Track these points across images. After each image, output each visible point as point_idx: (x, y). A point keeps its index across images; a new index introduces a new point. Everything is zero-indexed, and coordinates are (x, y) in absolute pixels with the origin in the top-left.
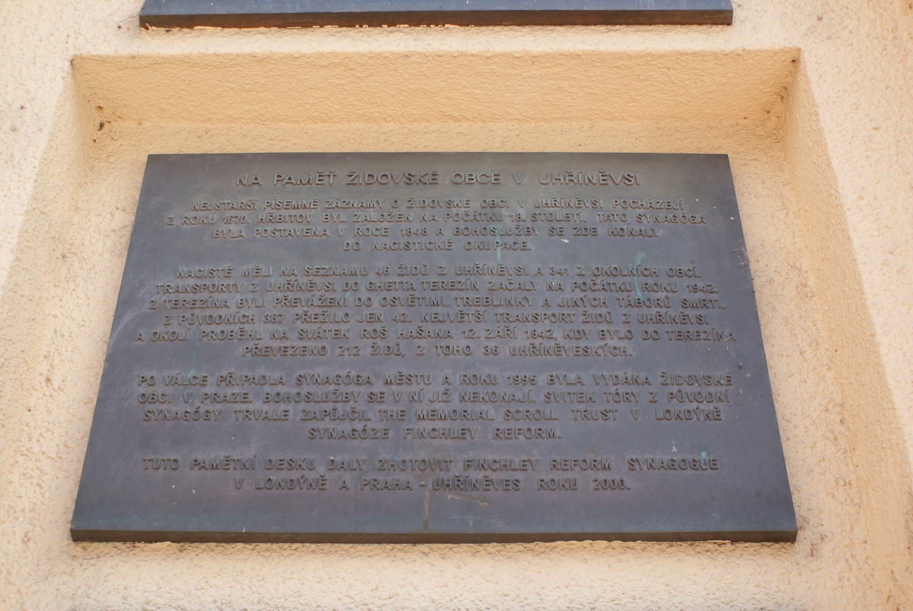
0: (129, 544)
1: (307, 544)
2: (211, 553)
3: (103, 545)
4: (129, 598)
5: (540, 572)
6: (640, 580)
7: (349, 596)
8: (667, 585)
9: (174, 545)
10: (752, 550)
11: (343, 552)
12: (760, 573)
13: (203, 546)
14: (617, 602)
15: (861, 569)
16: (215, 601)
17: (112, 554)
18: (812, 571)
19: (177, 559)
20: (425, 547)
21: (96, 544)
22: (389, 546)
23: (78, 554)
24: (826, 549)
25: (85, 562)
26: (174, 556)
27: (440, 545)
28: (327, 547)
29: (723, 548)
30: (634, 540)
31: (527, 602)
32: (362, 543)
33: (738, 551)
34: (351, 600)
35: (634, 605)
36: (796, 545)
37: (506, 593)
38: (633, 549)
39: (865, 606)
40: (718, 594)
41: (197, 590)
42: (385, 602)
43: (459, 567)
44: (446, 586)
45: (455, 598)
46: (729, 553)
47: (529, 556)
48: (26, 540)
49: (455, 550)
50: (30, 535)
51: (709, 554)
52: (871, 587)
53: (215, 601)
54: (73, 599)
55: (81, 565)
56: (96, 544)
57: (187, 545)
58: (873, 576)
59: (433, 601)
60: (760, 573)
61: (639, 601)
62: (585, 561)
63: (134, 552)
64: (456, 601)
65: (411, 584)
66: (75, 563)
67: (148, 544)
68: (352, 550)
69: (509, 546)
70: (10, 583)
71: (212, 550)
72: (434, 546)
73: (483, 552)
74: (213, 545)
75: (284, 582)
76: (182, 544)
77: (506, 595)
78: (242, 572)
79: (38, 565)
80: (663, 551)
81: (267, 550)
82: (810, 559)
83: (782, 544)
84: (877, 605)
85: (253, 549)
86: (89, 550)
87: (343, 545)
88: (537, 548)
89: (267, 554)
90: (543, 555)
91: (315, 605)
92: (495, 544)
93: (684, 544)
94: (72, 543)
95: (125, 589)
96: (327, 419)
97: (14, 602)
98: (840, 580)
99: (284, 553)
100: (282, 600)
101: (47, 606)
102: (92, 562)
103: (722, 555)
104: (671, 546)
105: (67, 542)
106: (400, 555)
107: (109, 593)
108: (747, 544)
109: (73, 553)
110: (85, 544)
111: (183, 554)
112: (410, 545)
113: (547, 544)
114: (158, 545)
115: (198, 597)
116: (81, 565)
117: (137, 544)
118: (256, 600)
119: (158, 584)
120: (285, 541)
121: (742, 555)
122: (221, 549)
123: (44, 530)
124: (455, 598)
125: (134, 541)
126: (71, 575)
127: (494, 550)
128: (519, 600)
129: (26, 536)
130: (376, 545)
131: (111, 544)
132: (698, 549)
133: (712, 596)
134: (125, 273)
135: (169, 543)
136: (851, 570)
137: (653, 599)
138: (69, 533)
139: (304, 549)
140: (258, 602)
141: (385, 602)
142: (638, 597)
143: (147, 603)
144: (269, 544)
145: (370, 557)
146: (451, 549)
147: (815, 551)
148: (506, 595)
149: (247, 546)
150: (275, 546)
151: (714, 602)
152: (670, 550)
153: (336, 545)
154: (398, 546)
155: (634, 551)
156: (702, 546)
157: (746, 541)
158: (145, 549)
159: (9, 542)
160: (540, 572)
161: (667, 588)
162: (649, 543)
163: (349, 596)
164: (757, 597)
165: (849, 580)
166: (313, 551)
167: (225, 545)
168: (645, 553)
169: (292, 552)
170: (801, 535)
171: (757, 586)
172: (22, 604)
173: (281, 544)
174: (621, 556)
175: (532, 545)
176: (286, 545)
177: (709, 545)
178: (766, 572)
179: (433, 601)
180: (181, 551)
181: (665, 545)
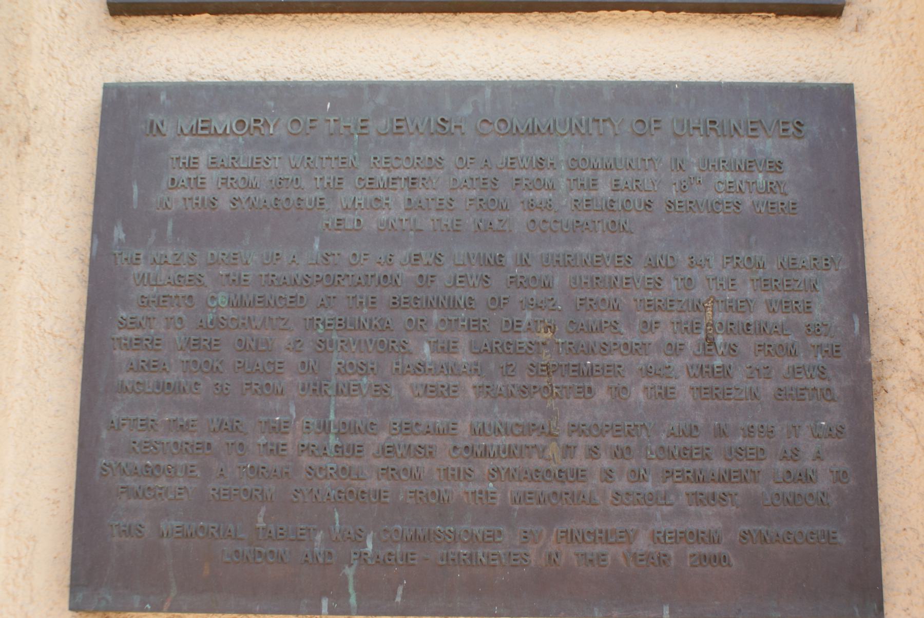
0: (167, 18)
1: (347, 14)
2: (251, 25)
3: (141, 19)
4: (173, 70)
5: (581, 42)
6: (682, 51)
7: (391, 64)
8: (708, 57)
9: (213, 17)
10: (796, 24)
11: (383, 22)
12: (802, 47)
13: (242, 18)
14: (657, 71)
15: (903, 45)
16: (258, 71)
17: (151, 27)
18: (855, 46)
19: (217, 31)
20: (466, 17)
21: (134, 19)
22: (430, 16)
23: (118, 28)
24: (871, 25)
25: (125, 36)
26: (214, 28)
27: (481, 15)
28: (367, 16)
29: (767, 22)
30: (678, 11)
31: (567, 70)
32: (403, 12)
33: (782, 25)
34: (393, 69)
35: (674, 74)
36: (842, 20)
37: (547, 61)
38: (676, 20)
39: (904, 81)
40: (758, 66)
41: (239, 60)
42: (427, 70)
43: (500, 36)
44: (487, 54)
45: (497, 65)
46: (772, 27)
47: (571, 25)
48: (63, 16)
49: (497, 19)
50: (66, 10)
51: (752, 27)
52: (912, 63)
53: (258, 71)
54: (117, 71)
55: (122, 38)
56: (134, 18)
57: (226, 17)
58: (915, 52)
59: (474, 69)
60: (802, 47)
61: (679, 71)
62: (627, 31)
63: (173, 25)
64: (496, 69)
65: (452, 52)
66: (116, 38)
67: (186, 17)
68: (393, 20)
69: (551, 16)
70: (53, 58)
71: (252, 22)
72: (475, 15)
73: (524, 22)
74: (251, 16)
75: (325, 51)
76: (221, 16)
77: (547, 64)
78: (283, 43)
79: (78, 40)
80: (706, 23)
81: (307, 21)
82: (854, 34)
83: (827, 18)
84: (915, 80)
85: (292, 20)
86: (127, 24)
87: (383, 15)
88: (579, 18)
89: (307, 24)
90: (585, 25)
91: (357, 73)
92: (536, 13)
93: (728, 17)
94: (110, 17)
95: (168, 61)
96: (320, 285)
97: (59, 76)
98: (882, 56)
99: (324, 23)
100: (325, 69)
101: (92, 79)
102: (133, 35)
103: (766, 28)
104: (715, 18)
105: (104, 16)
106: (441, 24)
107: (153, 65)
108: (793, 18)
109: (111, 27)
110: (123, 18)
111: (222, 27)
112: (451, 15)
113: (590, 14)
114: (197, 17)
115: (241, 67)
116: (122, 38)
117: (175, 17)
118: (298, 69)
119: (200, 56)
120: (324, 11)
121: (785, 29)
122: (260, 20)
123: (80, 6)
124: (497, 65)
125: (171, 15)
126: (112, 48)
127: (535, 20)
128: (560, 68)
129: (62, 11)
130: (417, 15)
131: (149, 18)
132: (743, 22)
133: (752, 68)
134: (73, 549)
135: (207, 15)
136: (894, 45)
137: (693, 69)
138: (106, 6)
139: (344, 19)
140: (301, 71)
141: (427, 70)
142: (678, 67)
143: (191, 74)
144: (309, 15)
145: (411, 26)
146: (492, 18)
147: (859, 27)
148: (547, 64)
149: (286, 17)
150: (314, 16)
151: (753, 73)
152: (714, 22)
153: (376, 15)
154: (439, 15)
155: (676, 23)
156: (746, 18)
157: (791, 15)
158: (184, 22)
159: (46, 18)
160: (581, 42)
161: (708, 59)
162: (693, 15)
163: (391, 64)
164: (797, 70)
165: (890, 56)
166: (353, 21)
167: (265, 16)
168: (687, 25)
169: (332, 22)
170: (847, 10)
171: (798, 59)
172: (68, 77)
173: (320, 15)
174: (663, 28)
175: (574, 15)
176: (326, 16)
177: (754, 18)
178: (808, 46)
179: (474, 69)
180: (220, 23)
181: (708, 17)
